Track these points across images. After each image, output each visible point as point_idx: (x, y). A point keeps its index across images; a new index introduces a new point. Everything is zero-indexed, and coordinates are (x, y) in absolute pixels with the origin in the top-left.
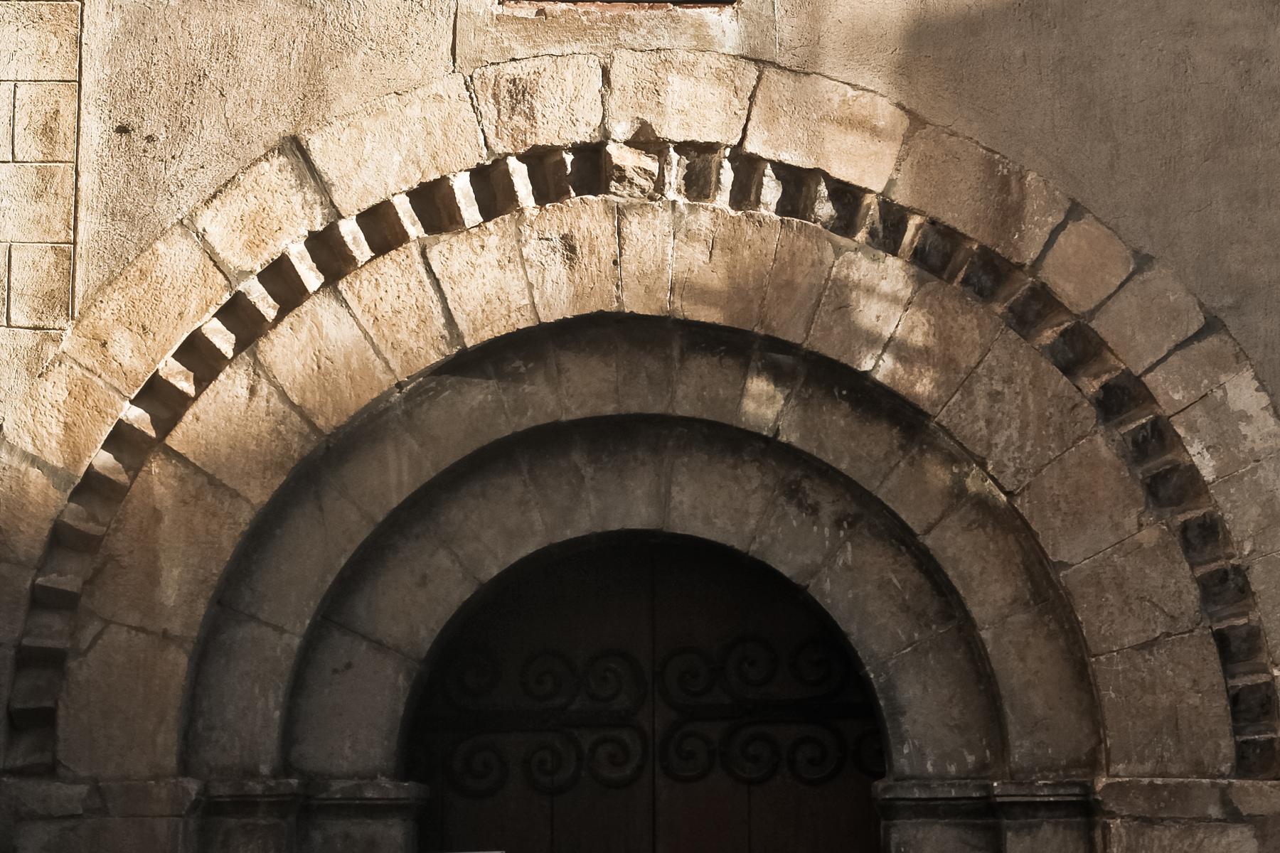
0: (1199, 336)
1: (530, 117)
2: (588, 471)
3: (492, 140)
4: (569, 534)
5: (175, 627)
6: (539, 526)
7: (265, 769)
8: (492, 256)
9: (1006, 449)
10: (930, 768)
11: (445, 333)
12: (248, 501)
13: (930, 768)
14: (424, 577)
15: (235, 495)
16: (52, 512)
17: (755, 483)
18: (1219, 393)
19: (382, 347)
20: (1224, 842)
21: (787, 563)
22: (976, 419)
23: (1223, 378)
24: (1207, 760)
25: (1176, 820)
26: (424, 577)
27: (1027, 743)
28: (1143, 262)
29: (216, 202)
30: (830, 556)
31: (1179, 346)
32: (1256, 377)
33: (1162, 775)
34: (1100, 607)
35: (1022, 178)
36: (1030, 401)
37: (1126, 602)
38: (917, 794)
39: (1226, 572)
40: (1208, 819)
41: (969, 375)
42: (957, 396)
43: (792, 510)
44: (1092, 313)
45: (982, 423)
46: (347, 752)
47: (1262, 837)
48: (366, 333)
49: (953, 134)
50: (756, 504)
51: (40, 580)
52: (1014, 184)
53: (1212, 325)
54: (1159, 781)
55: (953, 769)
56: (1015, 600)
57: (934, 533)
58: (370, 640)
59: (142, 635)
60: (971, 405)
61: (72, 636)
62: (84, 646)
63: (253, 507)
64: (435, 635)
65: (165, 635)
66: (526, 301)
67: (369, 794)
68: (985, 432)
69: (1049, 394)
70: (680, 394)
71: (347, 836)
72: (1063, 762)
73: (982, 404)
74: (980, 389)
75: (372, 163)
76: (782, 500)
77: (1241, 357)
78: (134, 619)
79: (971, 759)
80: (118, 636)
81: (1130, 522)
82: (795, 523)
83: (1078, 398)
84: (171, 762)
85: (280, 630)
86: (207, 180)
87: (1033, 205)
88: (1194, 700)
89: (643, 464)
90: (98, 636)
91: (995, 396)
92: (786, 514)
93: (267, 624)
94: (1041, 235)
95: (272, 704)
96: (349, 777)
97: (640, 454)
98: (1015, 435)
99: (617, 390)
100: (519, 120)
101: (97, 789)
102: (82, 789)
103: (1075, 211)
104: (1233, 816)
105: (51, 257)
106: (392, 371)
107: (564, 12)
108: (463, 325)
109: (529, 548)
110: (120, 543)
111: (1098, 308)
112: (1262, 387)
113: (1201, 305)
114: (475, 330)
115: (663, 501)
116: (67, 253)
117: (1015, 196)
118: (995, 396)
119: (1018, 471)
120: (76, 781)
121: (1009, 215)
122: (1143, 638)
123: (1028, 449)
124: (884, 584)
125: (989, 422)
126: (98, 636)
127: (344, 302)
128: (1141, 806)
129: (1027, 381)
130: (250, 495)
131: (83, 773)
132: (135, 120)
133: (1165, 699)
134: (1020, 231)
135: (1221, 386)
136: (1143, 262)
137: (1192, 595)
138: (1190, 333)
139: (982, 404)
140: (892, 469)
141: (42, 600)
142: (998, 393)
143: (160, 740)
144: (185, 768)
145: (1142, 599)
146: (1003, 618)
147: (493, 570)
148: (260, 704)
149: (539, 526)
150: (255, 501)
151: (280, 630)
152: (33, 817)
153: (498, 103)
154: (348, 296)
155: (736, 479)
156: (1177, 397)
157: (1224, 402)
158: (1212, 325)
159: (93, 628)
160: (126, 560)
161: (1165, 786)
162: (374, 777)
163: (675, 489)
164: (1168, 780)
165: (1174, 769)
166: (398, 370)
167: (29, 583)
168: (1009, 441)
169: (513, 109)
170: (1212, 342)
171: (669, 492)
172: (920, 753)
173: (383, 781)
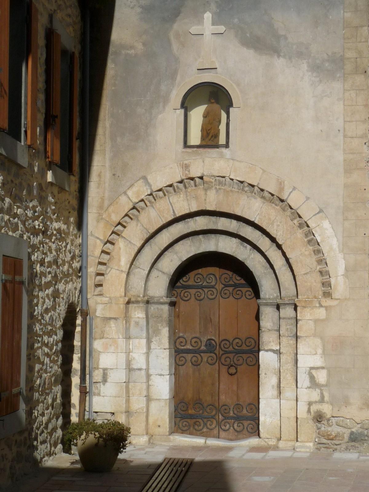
0: (318, 213)
1: (189, 171)
2: (203, 240)
3: (182, 176)
4: (199, 252)
5: (124, 270)
6: (193, 250)
7: (141, 296)
8: (182, 199)
9: (280, 236)
10: (267, 297)
11: (173, 214)
12: (136, 246)
13: (267, 297)
14: (172, 260)
15: (134, 245)
16: (260, 199)
17: (235, 242)
18: (322, 225)
19: (161, 216)
20: (319, 311)
21: (241, 257)
22: (274, 230)
23: (322, 221)
24: (317, 295)
25: (310, 307)
26: (172, 260)
27: (284, 292)
28: (308, 198)
29: (130, 189)
30: (249, 256)
31: (314, 215)
32: (329, 221)
33: (307, 298)
34: (297, 266)
35: (284, 183)
36: (285, 226)
37: (302, 266)
38: (264, 301)
39: (322, 259)
40: (316, 307)
41: (273, 222)
42: (271, 226)
43: (242, 247)
44: (297, 209)
45: (275, 231)
46: (158, 293)
47: (326, 310)
48: (158, 214)
49: (271, 174)
50: (235, 246)
51: (100, 260)
52: (282, 184)
53: (321, 211)
54: (306, 300)
55: (272, 297)
56: (283, 265)
57: (267, 252)
58: (162, 272)
59: (118, 271)
60: (273, 227)
61: (106, 271)
62: (107, 273)
63: (137, 247)
64: (174, 271)
65: (122, 271)
66: (188, 208)
67: (161, 301)
68: (276, 232)
69: (288, 225)
70: (219, 225)
71: (158, 308)
72: (291, 296)
73: (275, 227)
74: (275, 224)
75: (159, 180)
76: (240, 245)
77: (326, 217)
78: (116, 268)
79: (275, 295)
80: (113, 271)
81: (303, 250)
82: (242, 250)
83: (294, 226)
84: (123, 294)
85: (144, 270)
86: (128, 184)
87: (286, 188)
88: (315, 284)
89: (213, 238)
90: (110, 271)
91: (278, 226)
92: (240, 248)
93: (142, 269)
94: (288, 194)
95: (143, 284)
96: (158, 297)
97: (212, 236)
98: (282, 233)
99: (207, 225)
100: (187, 172)
101: (110, 298)
102: (108, 299)
103: (294, 189)
104: (321, 306)
105: (100, 200)
106: (163, 221)
107: (196, 150)
108: (176, 213)
109: (192, 255)
110: (113, 254)
111: (298, 208)
112: (330, 223)
113: (319, 207)
114: (178, 213)
115: (217, 245)
116: (103, 199)
117: (282, 186)
118: (278, 226)
119: (282, 240)
120: (107, 297)
121: (281, 189)
122: (305, 272)
123: (284, 236)
124: (259, 262)
125: (277, 231)
126: (110, 271)
127: (154, 208)
128: (303, 304)
129: (284, 222)
130: (137, 245)
131: (108, 296)
132: (116, 173)
133: (309, 284)
134: (283, 193)
135: (322, 223)
136: (308, 198)
137: (315, 263)
138: (316, 213)
139: (275, 227)
140: (259, 239)
141: (100, 263)
142: (279, 225)
143: (121, 290)
144: (125, 296)
145: (305, 265)
146: (280, 268)
147: (184, 259)
148: (140, 284)
149: (193, 250)
150: (138, 246)
151: (144, 270)
152: (99, 303)
153: (183, 169)
154: (154, 206)
155: (231, 241)
156: (313, 225)
157: (322, 226)
158: (321, 211)
159: (109, 269)
160: (115, 257)
161: (308, 300)
162: (162, 297)
163: (219, 243)
164: (309, 299)
165: (310, 297)
166: (164, 221)
167: (97, 261)
168: (280, 234)
169: (186, 170)
170: (321, 214)
171: (218, 244)
172: (266, 294)
173: (164, 298)
